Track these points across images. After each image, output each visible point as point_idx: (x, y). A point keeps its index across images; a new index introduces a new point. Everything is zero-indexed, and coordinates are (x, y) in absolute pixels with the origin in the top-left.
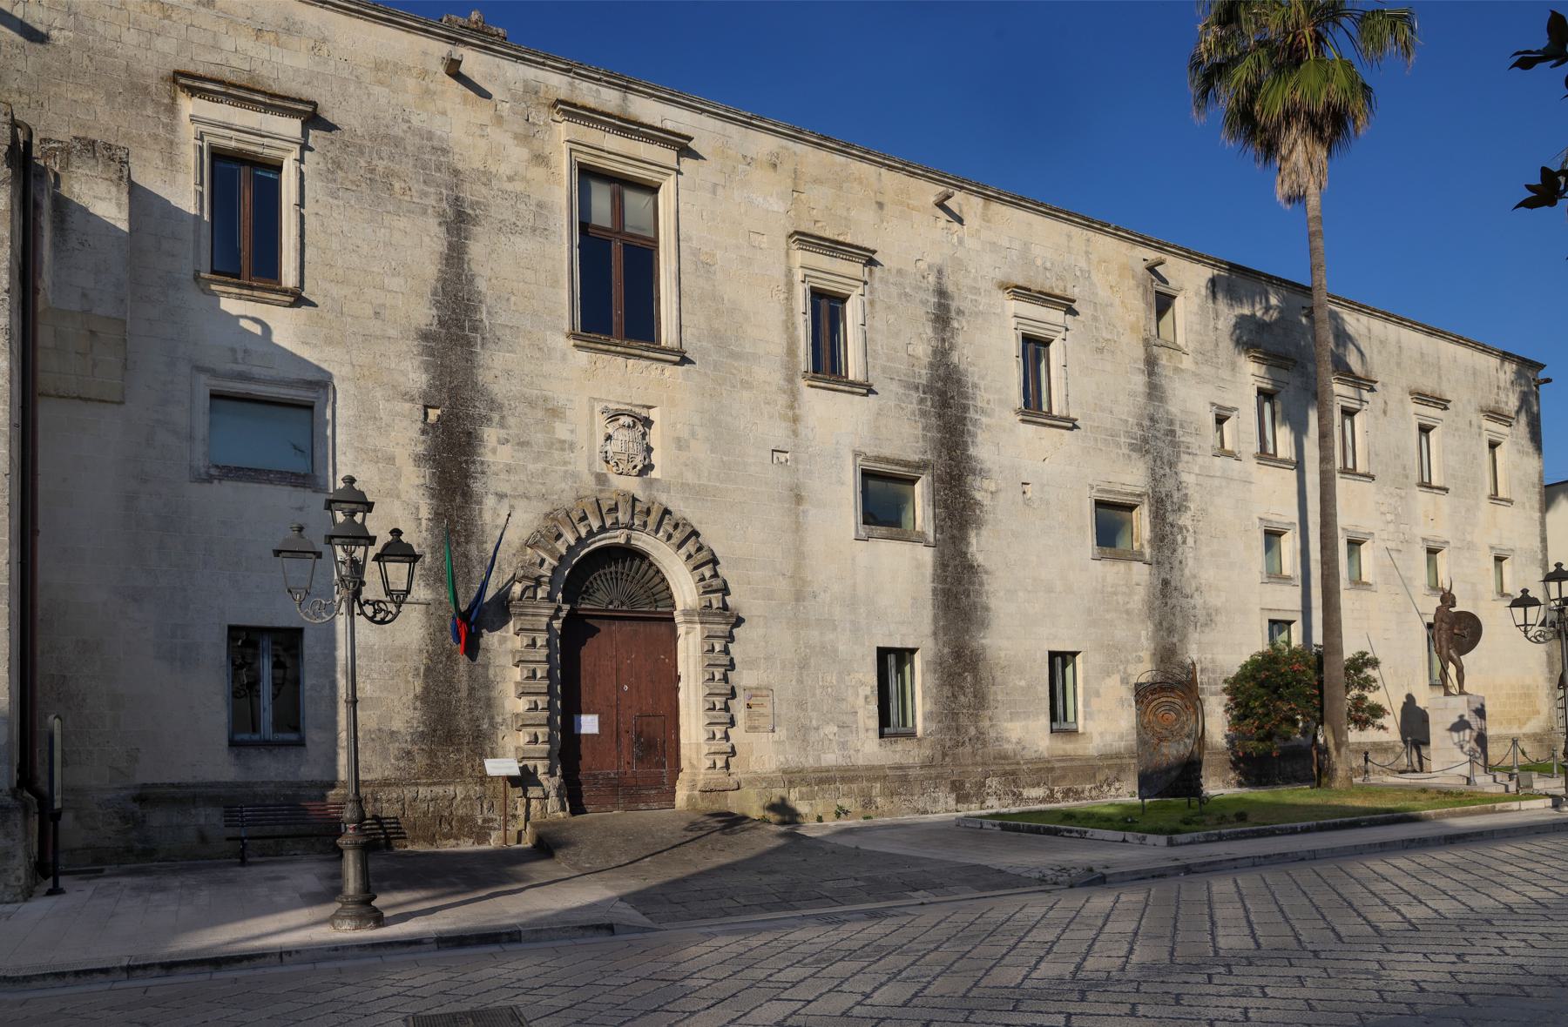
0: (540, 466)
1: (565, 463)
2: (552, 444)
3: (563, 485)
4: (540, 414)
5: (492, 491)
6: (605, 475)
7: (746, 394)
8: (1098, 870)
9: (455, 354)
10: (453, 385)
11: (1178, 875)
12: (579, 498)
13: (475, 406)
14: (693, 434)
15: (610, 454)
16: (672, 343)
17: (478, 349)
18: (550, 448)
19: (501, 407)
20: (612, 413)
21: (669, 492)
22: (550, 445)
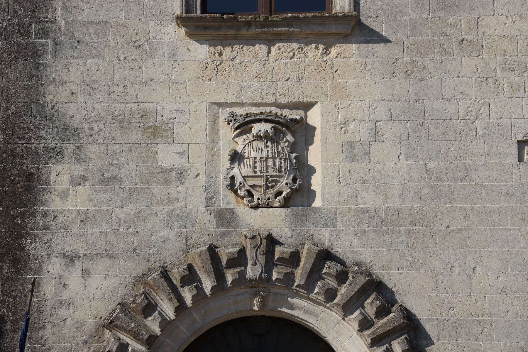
0: (131, 209)
1: (170, 200)
2: (151, 175)
3: (165, 233)
4: (134, 136)
5: (57, 252)
6: (232, 211)
7: (468, 63)
8: (228, 182)
9: (16, 71)
10: (10, 112)
11: (302, 39)
12: (186, 251)
13: (40, 137)
14: (376, 134)
15: (239, 179)
16: (342, 7)
17: (48, 59)
18: (149, 181)
19: (77, 133)
20: (240, 120)
21: (334, 225)
22: (149, 178)
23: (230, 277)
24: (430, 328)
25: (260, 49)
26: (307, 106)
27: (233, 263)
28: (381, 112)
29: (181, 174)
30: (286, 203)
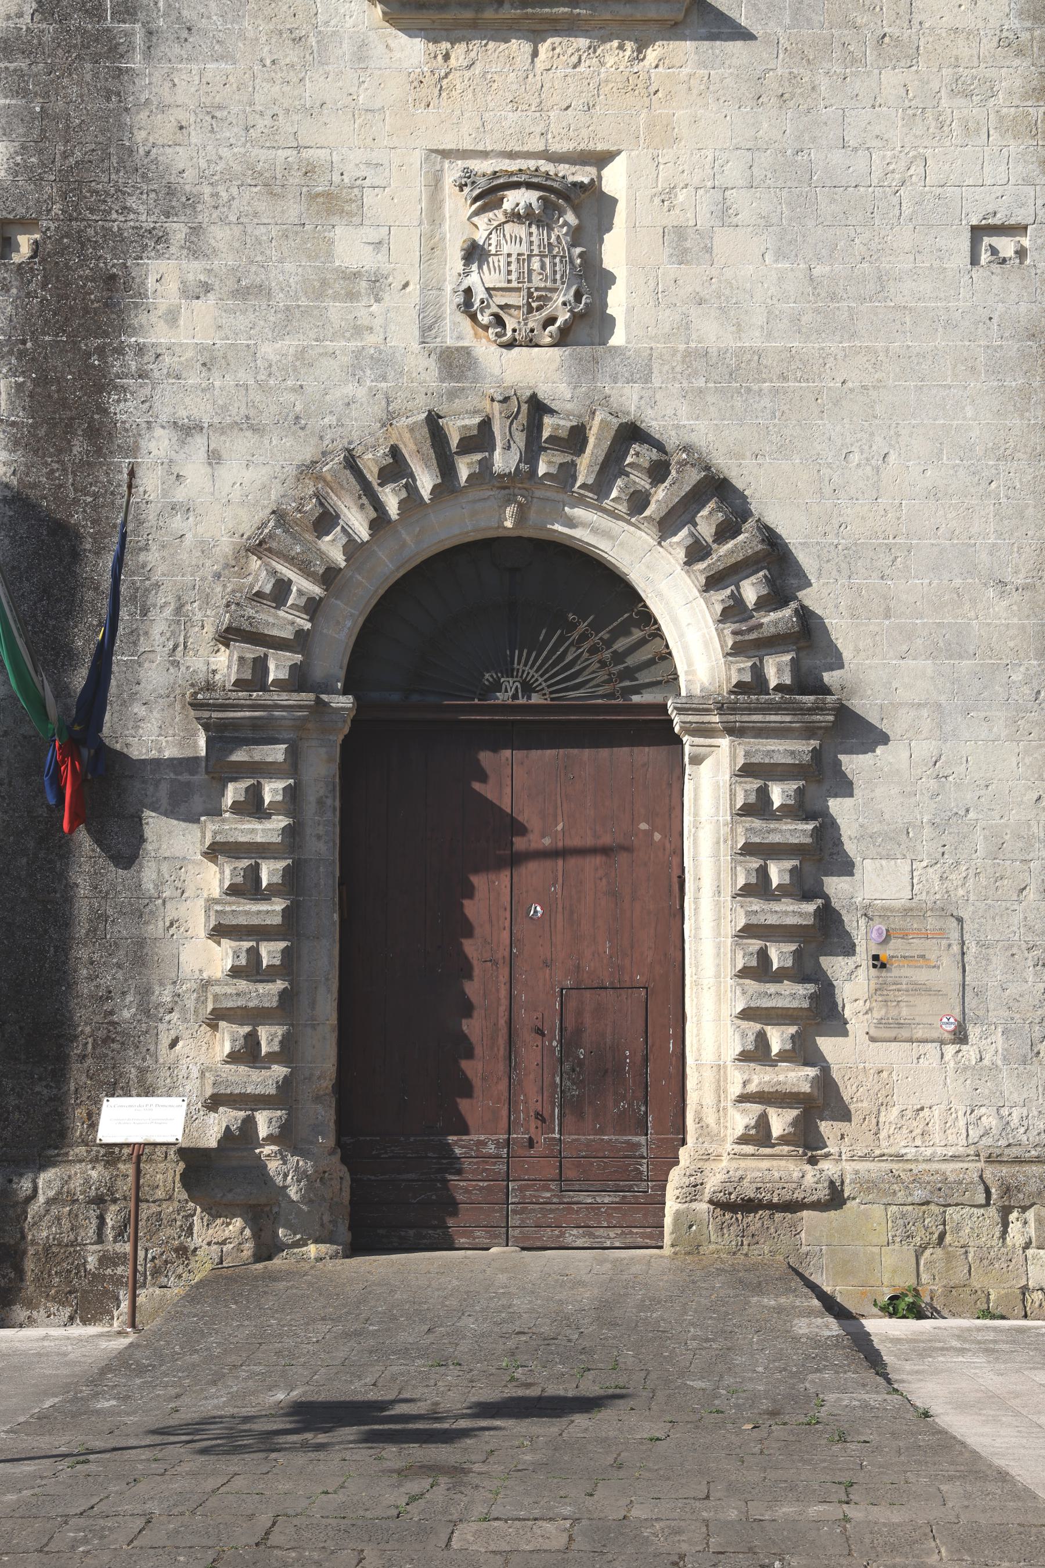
0: (290, 344)
1: (358, 331)
4: (293, 210)
14: (724, 213)
17: (138, 61)
19: (191, 202)
22: (320, 290)
23: (464, 469)
24: (804, 558)
25: (519, 48)
26: (602, 159)
27: (468, 445)
28: (734, 173)
29: (377, 283)
30: (563, 339)
